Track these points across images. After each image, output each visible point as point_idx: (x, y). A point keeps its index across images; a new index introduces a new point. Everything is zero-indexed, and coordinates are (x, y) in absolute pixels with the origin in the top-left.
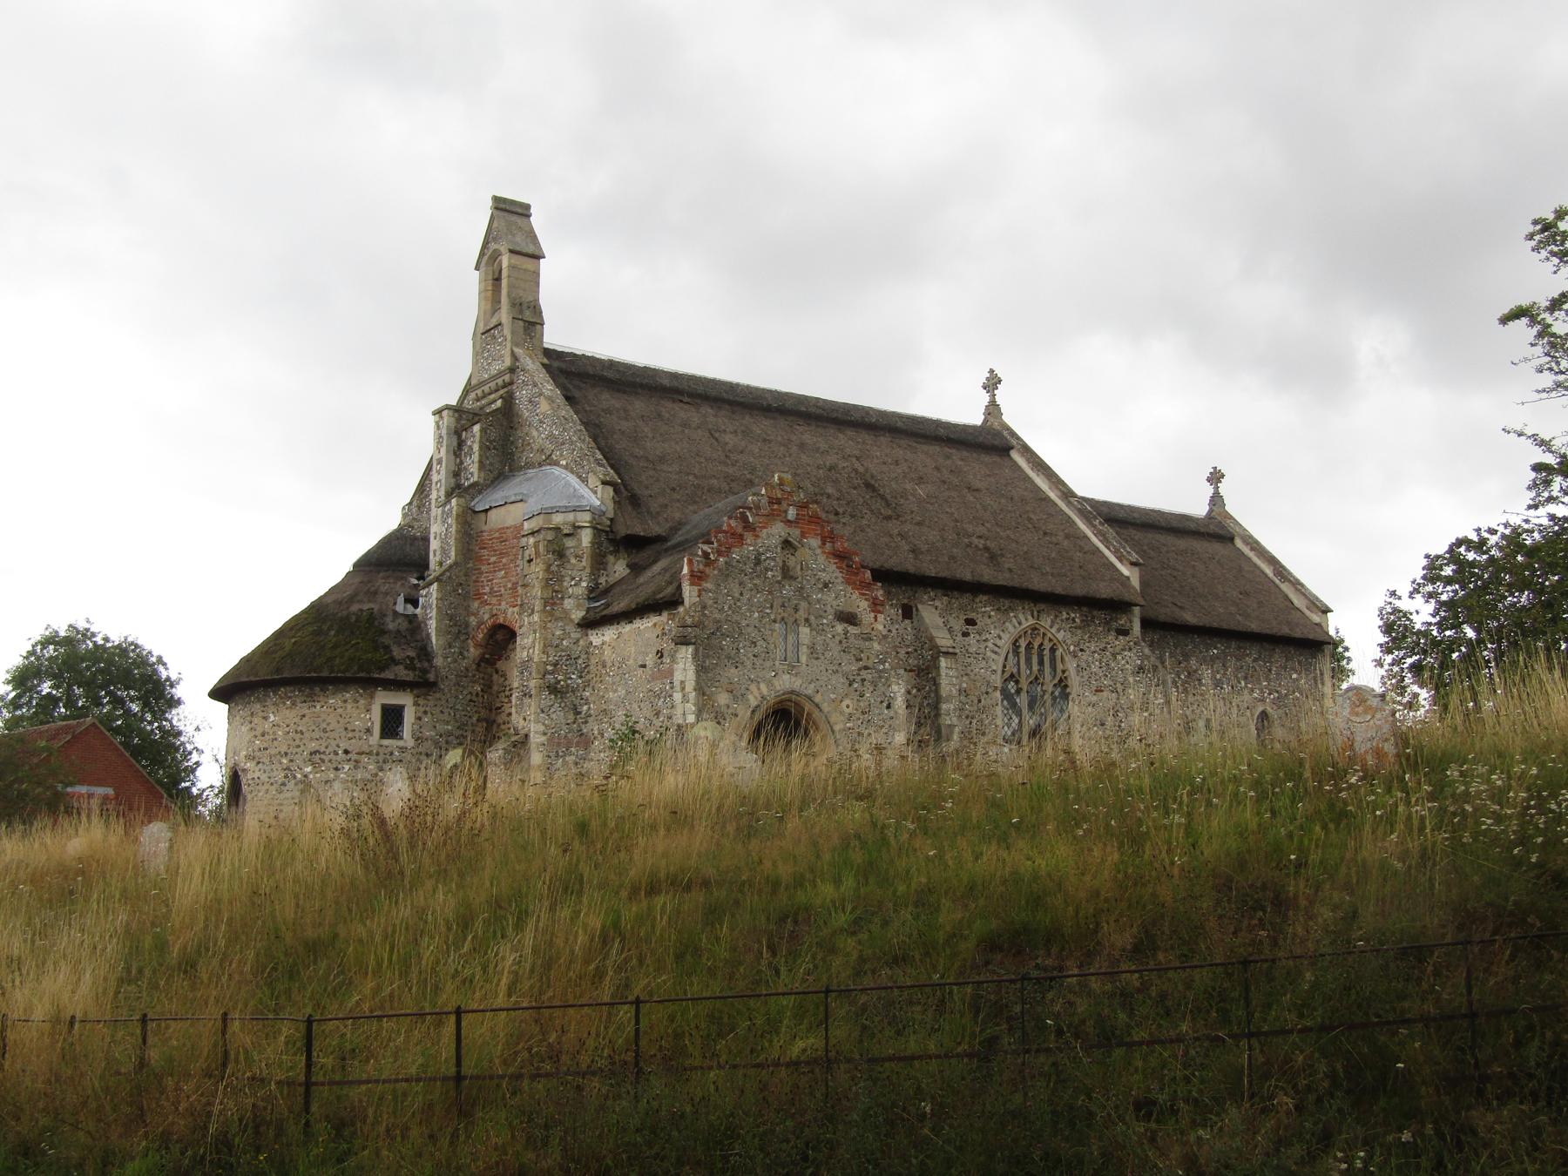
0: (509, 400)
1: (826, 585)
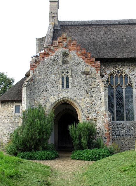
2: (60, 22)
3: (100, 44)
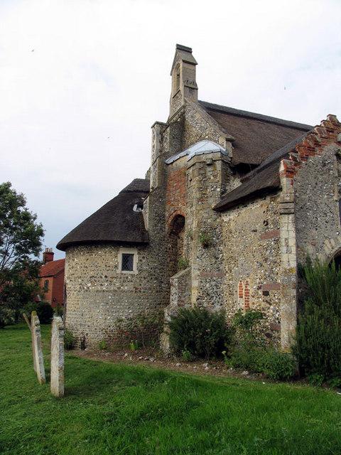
0: (184, 119)
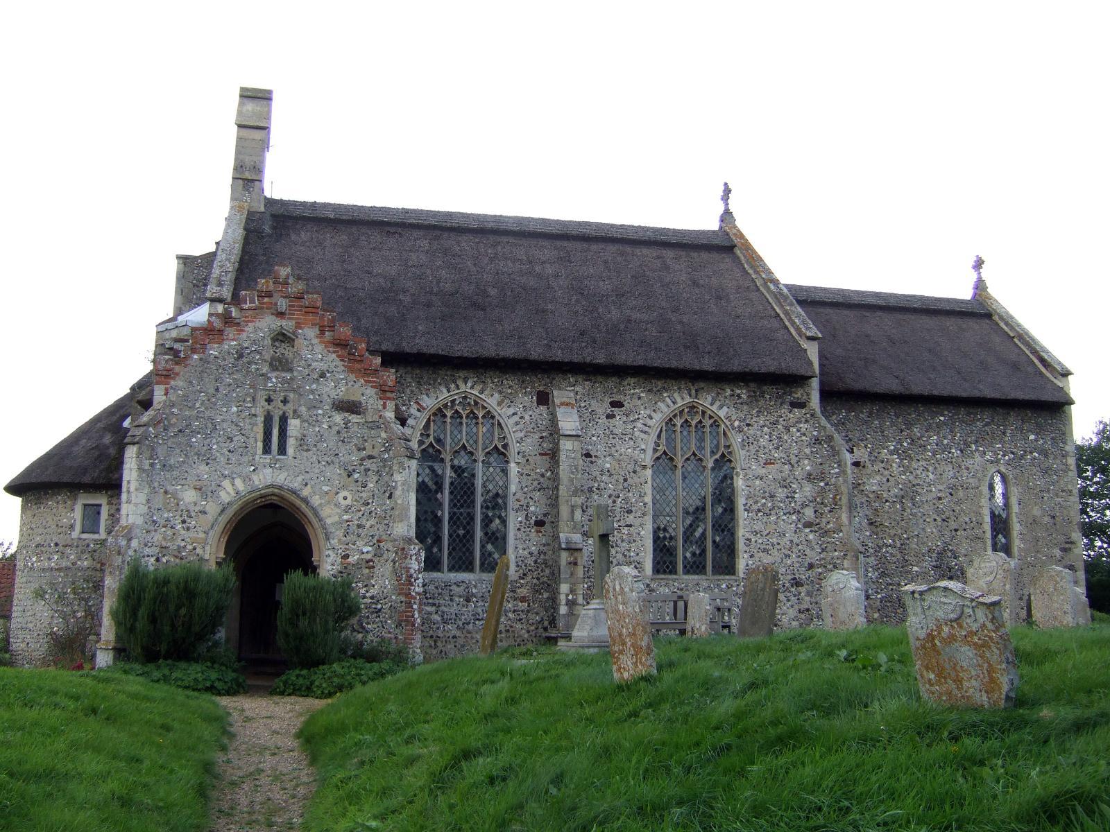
1: (323, 375)
2: (270, 202)
3: (408, 299)
